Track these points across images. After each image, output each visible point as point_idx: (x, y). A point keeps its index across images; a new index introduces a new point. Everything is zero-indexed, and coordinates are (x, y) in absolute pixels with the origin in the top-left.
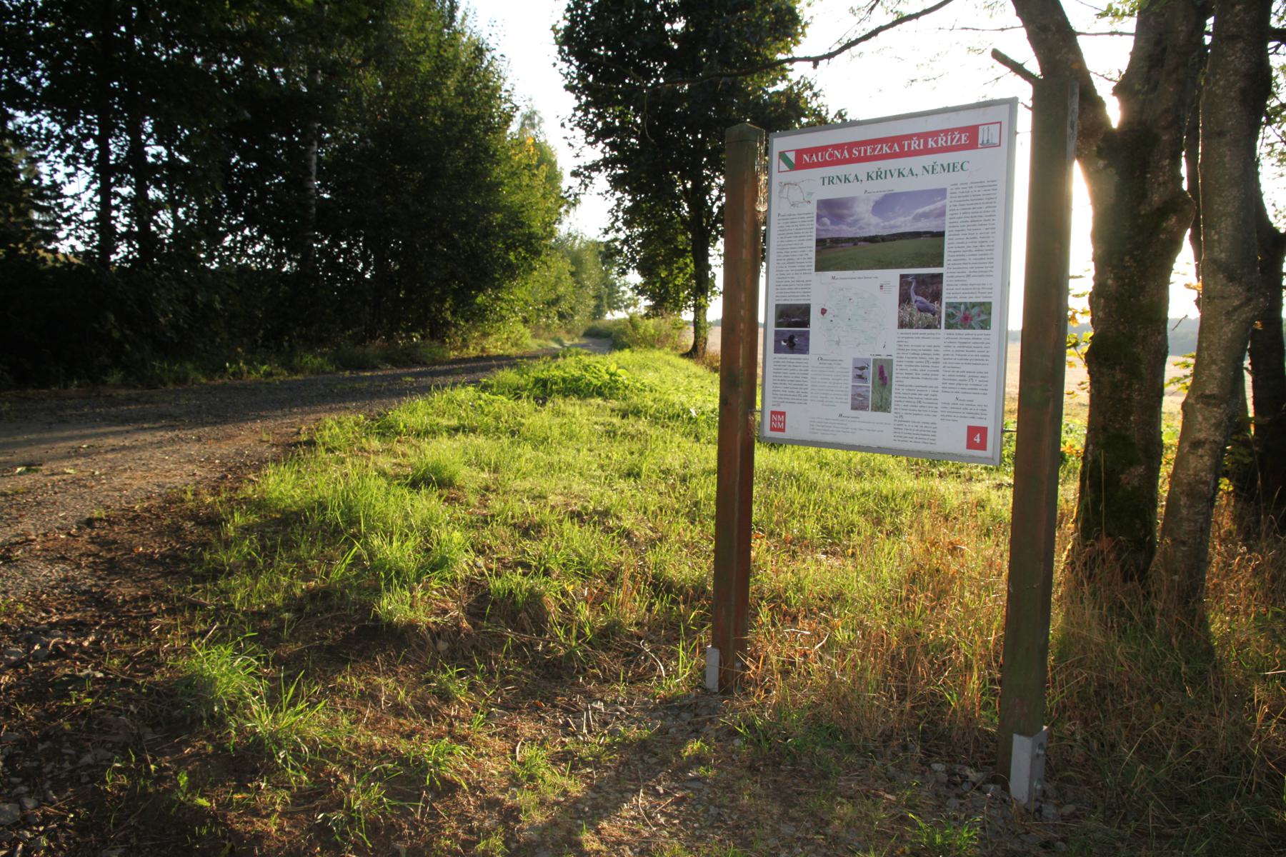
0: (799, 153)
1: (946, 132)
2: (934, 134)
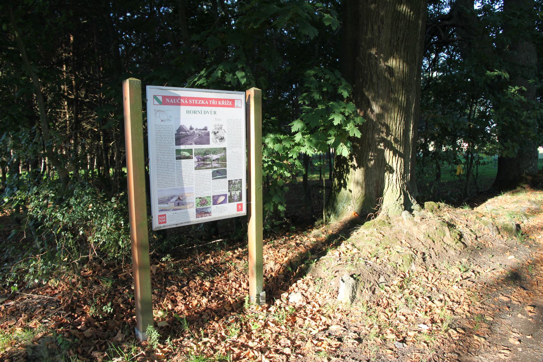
0: (164, 97)
1: (224, 100)
2: (221, 100)
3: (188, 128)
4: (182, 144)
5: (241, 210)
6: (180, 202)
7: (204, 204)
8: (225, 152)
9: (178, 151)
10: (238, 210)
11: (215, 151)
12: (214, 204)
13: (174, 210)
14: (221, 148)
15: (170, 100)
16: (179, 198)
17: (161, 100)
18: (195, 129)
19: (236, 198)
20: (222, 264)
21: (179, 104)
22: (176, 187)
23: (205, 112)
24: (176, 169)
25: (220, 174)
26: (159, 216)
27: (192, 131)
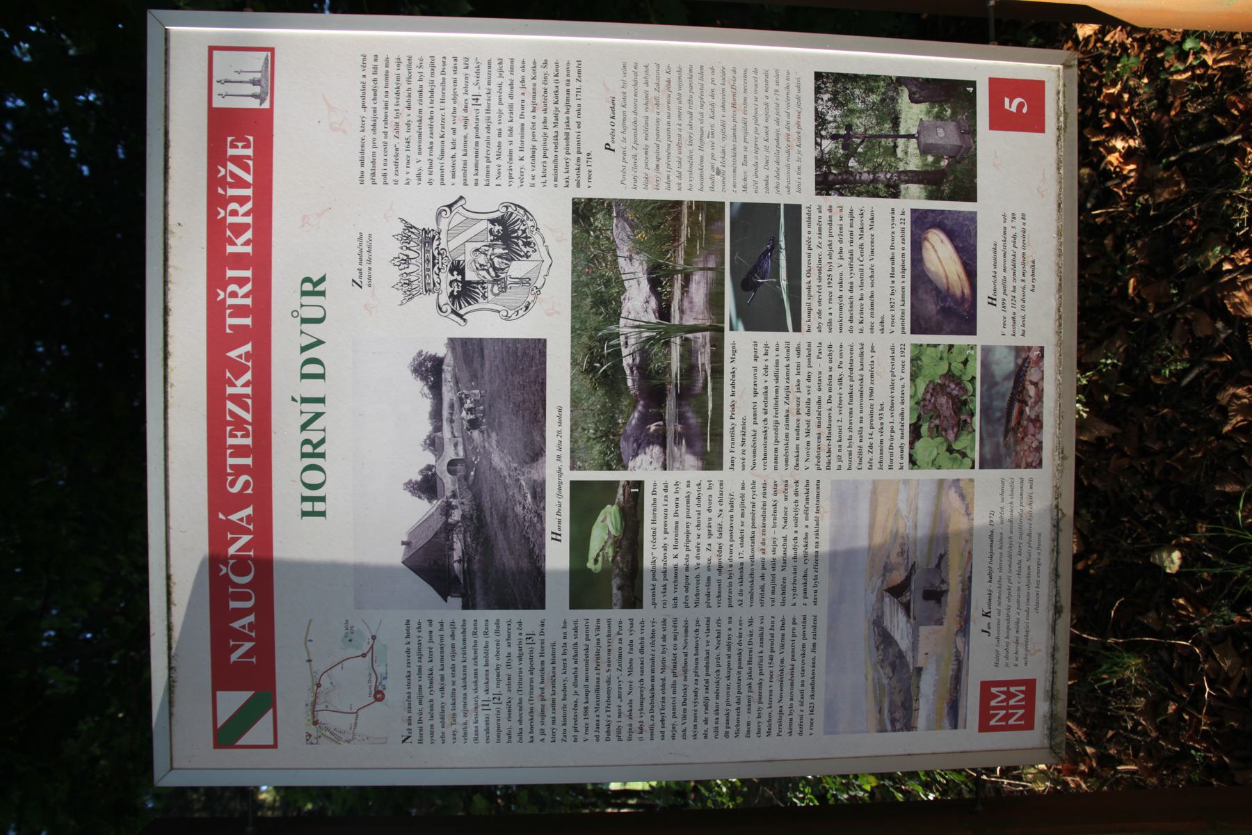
3: (423, 508)
4: (536, 557)
5: (1033, 91)
6: (921, 581)
7: (960, 405)
8: (606, 206)
9: (586, 589)
10: (1033, 122)
11: (596, 298)
12: (968, 324)
13: (964, 629)
14: (578, 247)
15: (241, 636)
16: (897, 591)
17: (243, 696)
18: (430, 458)
19: (945, 135)
20: (1164, 107)
21: (262, 567)
22: (822, 610)
23: (313, 369)
24: (702, 612)
25: (758, 259)
26: (984, 727)
27: (448, 482)
